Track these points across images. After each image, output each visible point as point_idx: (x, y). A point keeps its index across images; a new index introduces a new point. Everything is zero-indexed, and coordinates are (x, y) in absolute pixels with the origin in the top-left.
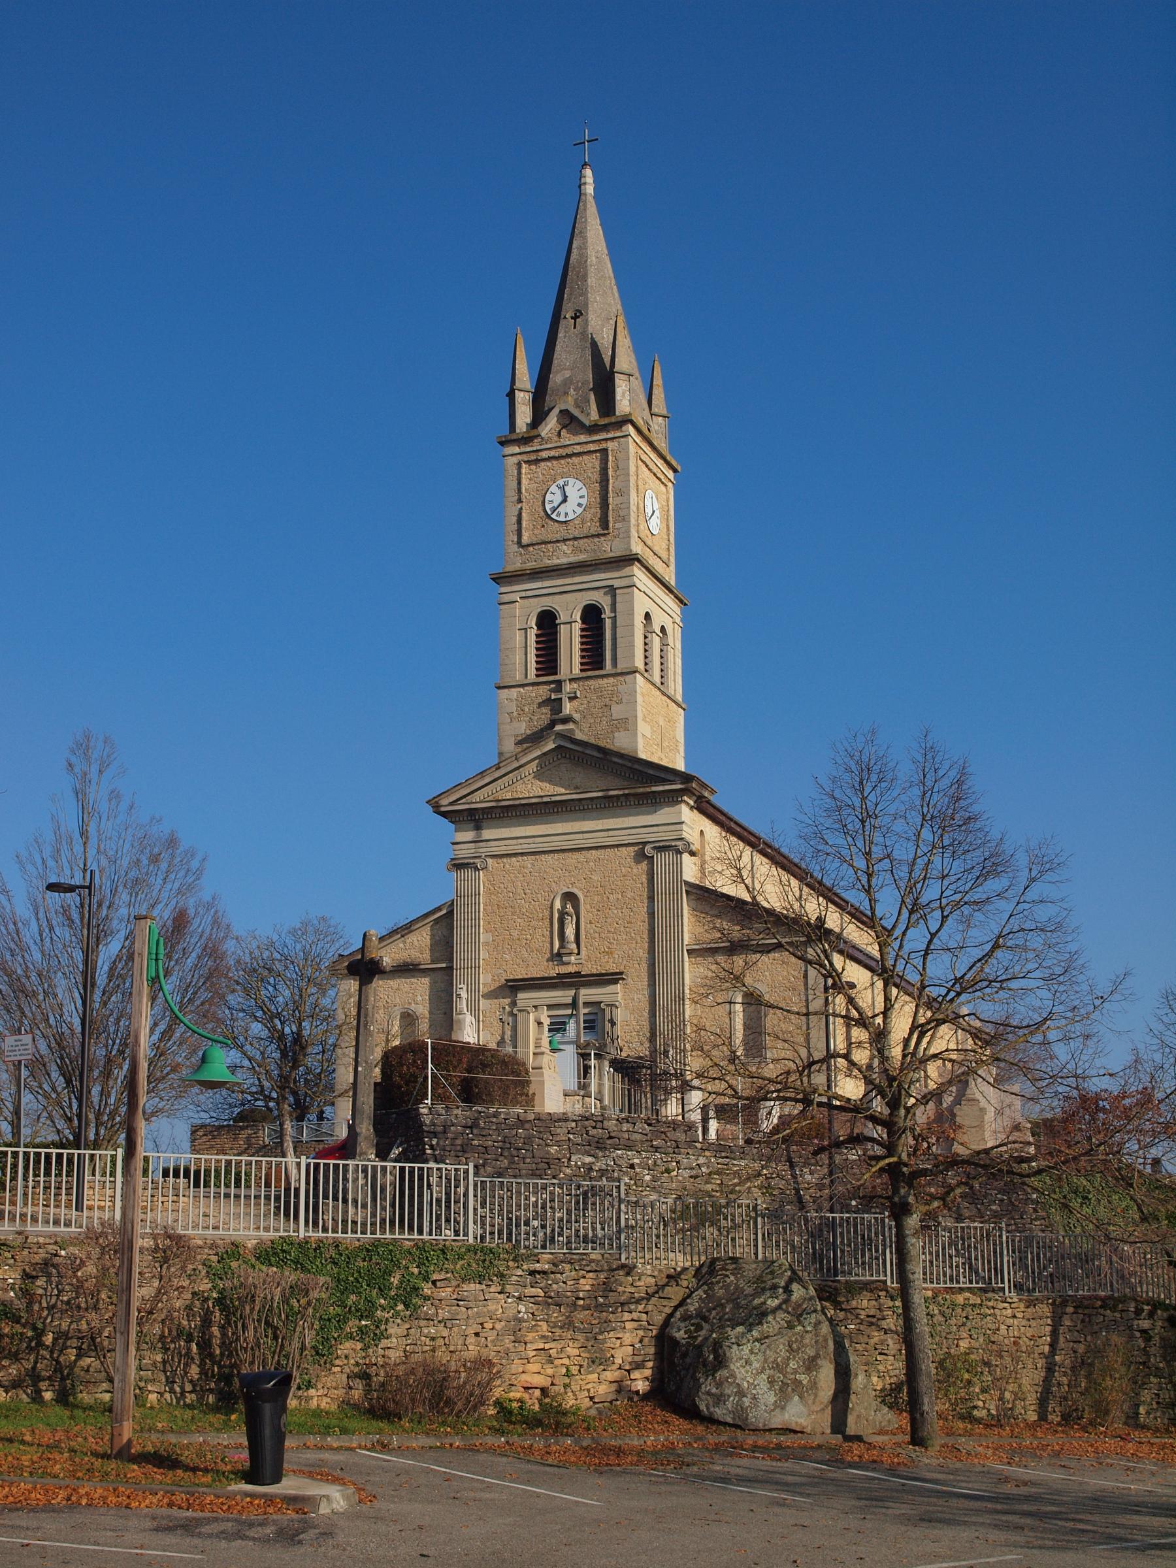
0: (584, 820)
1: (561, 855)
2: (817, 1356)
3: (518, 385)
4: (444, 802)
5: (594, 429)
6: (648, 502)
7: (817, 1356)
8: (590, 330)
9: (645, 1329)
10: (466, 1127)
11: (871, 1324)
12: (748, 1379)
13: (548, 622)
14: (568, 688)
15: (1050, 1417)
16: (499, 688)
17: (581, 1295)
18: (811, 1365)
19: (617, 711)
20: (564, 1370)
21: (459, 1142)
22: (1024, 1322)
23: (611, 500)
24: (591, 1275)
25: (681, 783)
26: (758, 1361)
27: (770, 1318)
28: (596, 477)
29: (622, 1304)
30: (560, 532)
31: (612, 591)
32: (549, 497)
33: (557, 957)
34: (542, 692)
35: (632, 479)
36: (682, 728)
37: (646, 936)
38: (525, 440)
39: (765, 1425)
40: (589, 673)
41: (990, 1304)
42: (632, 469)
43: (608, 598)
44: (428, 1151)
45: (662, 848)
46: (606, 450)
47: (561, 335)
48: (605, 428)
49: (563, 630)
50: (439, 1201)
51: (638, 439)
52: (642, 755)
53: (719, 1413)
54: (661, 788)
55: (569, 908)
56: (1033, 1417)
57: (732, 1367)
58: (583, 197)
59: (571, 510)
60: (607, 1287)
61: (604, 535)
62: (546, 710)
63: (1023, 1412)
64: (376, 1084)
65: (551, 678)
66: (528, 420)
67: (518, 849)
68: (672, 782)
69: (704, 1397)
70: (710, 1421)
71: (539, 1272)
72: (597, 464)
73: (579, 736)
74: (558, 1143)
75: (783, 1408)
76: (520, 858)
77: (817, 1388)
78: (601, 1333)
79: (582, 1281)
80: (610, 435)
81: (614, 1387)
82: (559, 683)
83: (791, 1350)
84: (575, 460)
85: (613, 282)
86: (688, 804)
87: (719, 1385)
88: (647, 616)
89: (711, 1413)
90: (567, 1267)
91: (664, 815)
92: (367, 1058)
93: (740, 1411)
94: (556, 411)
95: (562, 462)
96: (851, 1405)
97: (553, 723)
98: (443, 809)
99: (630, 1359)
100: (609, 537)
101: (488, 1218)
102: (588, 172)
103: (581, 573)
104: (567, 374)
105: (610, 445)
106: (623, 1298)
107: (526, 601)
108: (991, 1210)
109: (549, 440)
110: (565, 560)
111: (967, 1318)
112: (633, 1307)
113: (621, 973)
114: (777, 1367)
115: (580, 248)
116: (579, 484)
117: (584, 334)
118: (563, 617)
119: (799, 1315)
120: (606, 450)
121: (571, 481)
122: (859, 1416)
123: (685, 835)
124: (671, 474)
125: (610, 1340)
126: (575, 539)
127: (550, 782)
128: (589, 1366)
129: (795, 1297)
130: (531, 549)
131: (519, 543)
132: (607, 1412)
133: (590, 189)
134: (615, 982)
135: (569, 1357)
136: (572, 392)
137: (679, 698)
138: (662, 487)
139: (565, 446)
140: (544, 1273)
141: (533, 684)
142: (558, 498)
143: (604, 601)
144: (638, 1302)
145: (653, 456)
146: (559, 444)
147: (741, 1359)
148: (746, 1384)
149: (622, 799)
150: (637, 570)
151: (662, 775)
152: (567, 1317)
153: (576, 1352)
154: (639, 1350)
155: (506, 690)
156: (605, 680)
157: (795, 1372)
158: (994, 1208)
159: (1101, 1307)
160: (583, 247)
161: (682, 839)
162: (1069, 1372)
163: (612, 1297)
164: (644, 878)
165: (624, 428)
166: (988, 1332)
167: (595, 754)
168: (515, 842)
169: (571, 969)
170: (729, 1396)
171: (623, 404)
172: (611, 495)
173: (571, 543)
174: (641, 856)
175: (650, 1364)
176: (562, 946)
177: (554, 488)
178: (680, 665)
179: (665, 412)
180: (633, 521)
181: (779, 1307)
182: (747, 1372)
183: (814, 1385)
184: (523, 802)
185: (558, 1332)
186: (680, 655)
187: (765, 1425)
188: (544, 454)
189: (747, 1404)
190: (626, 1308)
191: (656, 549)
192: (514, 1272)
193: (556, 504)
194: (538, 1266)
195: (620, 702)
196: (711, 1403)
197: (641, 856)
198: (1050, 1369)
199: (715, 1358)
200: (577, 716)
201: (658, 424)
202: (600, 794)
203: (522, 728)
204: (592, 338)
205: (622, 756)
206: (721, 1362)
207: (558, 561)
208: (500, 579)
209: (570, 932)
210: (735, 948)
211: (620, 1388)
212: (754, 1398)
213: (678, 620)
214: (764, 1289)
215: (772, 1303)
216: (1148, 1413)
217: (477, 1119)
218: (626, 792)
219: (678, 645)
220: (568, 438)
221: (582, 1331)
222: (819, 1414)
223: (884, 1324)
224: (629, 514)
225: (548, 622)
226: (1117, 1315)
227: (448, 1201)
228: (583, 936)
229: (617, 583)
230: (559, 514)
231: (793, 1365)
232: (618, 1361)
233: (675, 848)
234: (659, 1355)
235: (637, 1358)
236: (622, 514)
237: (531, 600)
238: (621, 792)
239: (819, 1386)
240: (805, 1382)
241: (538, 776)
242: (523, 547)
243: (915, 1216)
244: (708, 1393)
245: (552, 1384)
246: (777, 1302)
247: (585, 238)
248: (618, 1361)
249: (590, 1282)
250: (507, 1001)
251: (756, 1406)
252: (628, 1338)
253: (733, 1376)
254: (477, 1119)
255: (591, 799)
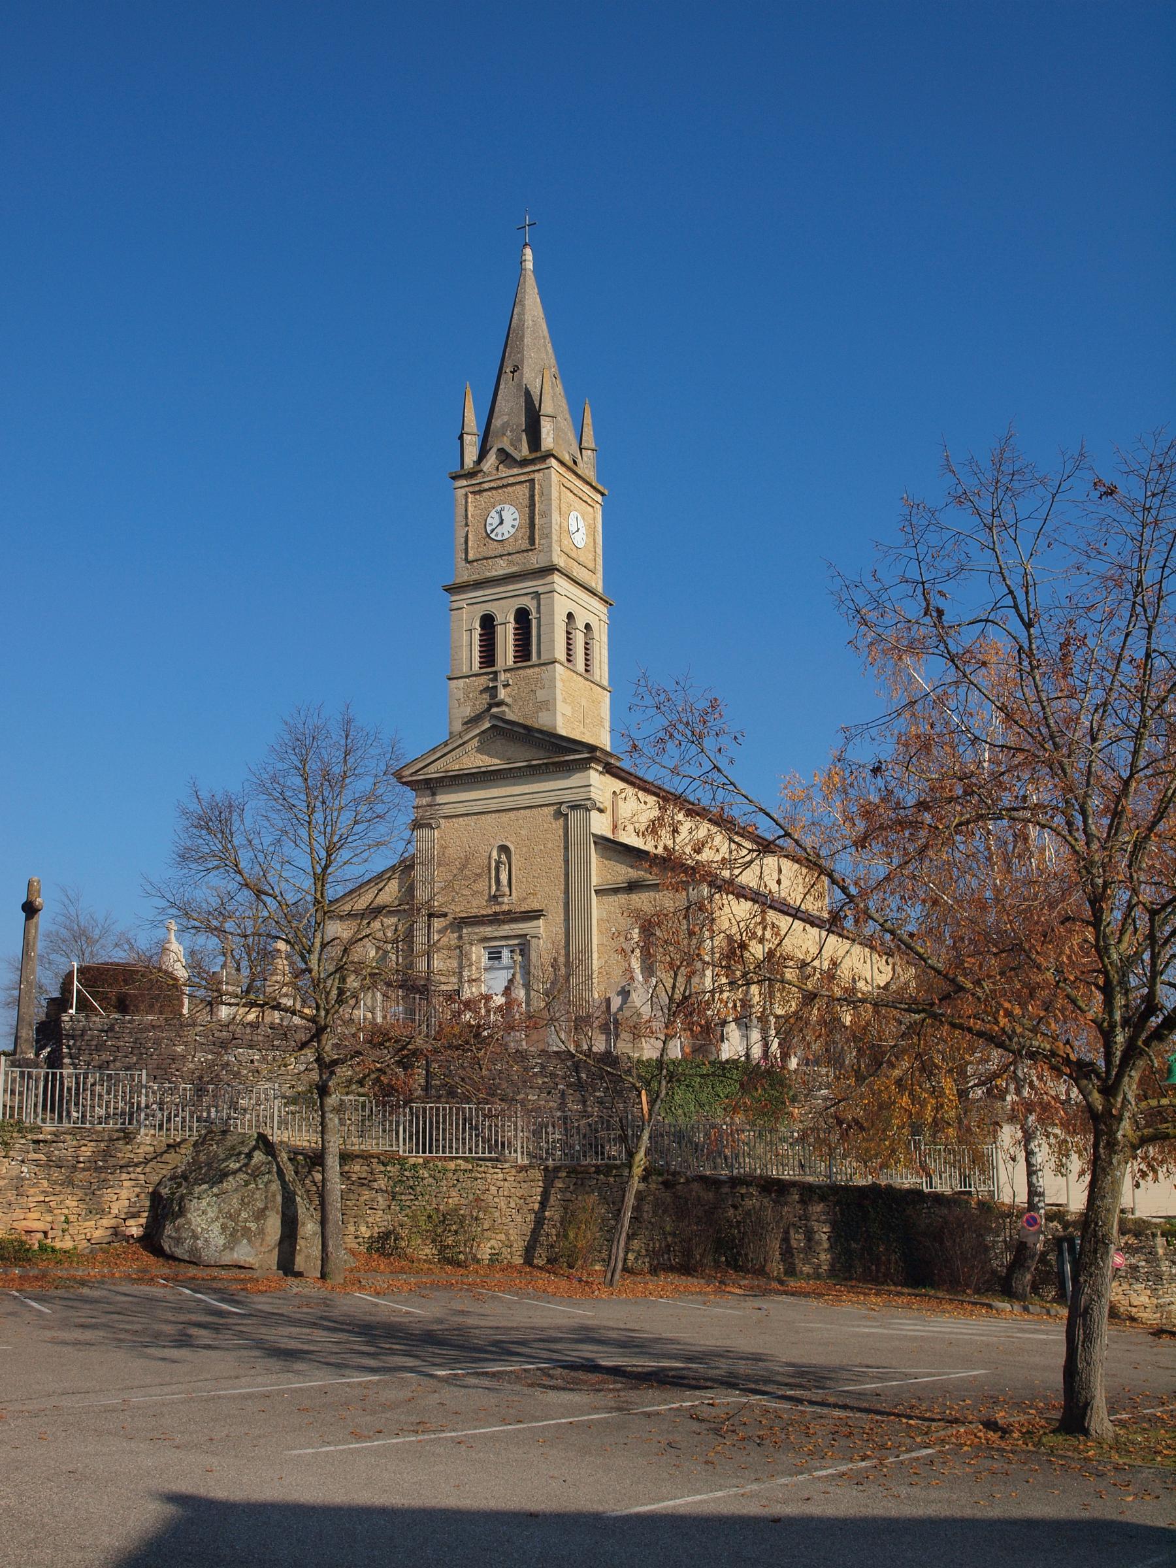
0: (514, 785)
1: (497, 815)
2: (266, 1208)
3: (466, 429)
4: (407, 773)
5: (524, 463)
6: (572, 521)
7: (266, 1208)
8: (525, 382)
9: (142, 1186)
10: (102, 1031)
11: (363, 1184)
12: (203, 1226)
13: (488, 623)
14: (502, 677)
15: (535, 1261)
16: (450, 679)
17: (81, 1159)
18: (260, 1215)
19: (541, 695)
20: (63, 1218)
21: (94, 1043)
22: (515, 1184)
23: (537, 521)
24: (92, 1144)
25: (589, 753)
26: (213, 1212)
27: (230, 1178)
28: (526, 502)
29: (121, 1167)
30: (496, 549)
31: (537, 596)
32: (489, 521)
33: (494, 898)
34: (483, 681)
35: (555, 504)
36: (608, 706)
37: (562, 880)
38: (472, 474)
39: (215, 1262)
40: (519, 665)
41: (481, 1169)
42: (555, 494)
43: (535, 602)
44: (65, 1050)
45: (574, 807)
46: (533, 480)
47: (502, 387)
48: (532, 462)
49: (499, 629)
50: (69, 1089)
51: (562, 470)
52: (562, 732)
53: (179, 1252)
54: (572, 757)
55: (503, 857)
56: (518, 1260)
57: (189, 1215)
58: (523, 272)
59: (506, 531)
60: (107, 1154)
61: (531, 550)
62: (486, 696)
63: (509, 1257)
64: (52, 1000)
65: (489, 670)
66: (475, 458)
67: (464, 810)
68: (581, 752)
69: (166, 1240)
70: (172, 1258)
71: (42, 1141)
72: (527, 491)
73: (510, 716)
74: (186, 1044)
75: (232, 1249)
76: (466, 818)
77: (264, 1234)
78: (99, 1189)
79: (83, 1148)
80: (537, 468)
81: (109, 1232)
82: (495, 673)
83: (243, 1203)
84: (510, 489)
85: (548, 339)
86: (597, 770)
87: (177, 1230)
88: (570, 616)
89: (173, 1253)
90: (68, 1137)
91: (576, 779)
92: (28, 977)
93: (194, 1250)
94: (494, 450)
95: (500, 491)
96: (298, 1248)
97: (491, 706)
98: (404, 780)
99: (126, 1210)
100: (535, 552)
101: (112, 1103)
102: (528, 252)
103: (513, 583)
104: (506, 418)
105: (537, 476)
106: (122, 1163)
107: (471, 607)
108: (594, 1096)
109: (490, 474)
110: (501, 572)
111: (458, 1181)
112: (131, 1169)
113: (542, 911)
114: (230, 1216)
115: (519, 314)
116: (513, 509)
117: (519, 385)
118: (499, 619)
119: (255, 1175)
120: (533, 480)
121: (507, 507)
122: (308, 1257)
123: (593, 795)
124: (599, 498)
125: (109, 1195)
126: (509, 554)
127: (489, 755)
128: (86, 1215)
129: (255, 1161)
130: (475, 564)
131: (466, 559)
132: (97, 1252)
133: (529, 265)
134: (537, 918)
135: (68, 1208)
136: (508, 433)
137: (605, 683)
138: (589, 508)
139: (502, 478)
140: (45, 1141)
141: (476, 675)
142: (497, 521)
143: (530, 604)
144: (137, 1165)
145: (579, 483)
146: (497, 477)
147: (198, 1210)
148: (199, 1230)
149: (543, 767)
150: (557, 578)
151: (572, 746)
152: (67, 1177)
153: (76, 1204)
154: (135, 1202)
155: (455, 681)
156: (532, 670)
157: (246, 1220)
158: (598, 1094)
159: (595, 1172)
160: (522, 313)
161: (590, 799)
162: (558, 1224)
163: (111, 1161)
164: (561, 832)
165: (548, 461)
166: (478, 1192)
167: (522, 731)
168: (461, 805)
169: (505, 908)
170: (186, 1239)
171: (548, 441)
172: (537, 517)
173: (506, 557)
174: (559, 814)
175: (146, 1214)
176: (497, 890)
177: (493, 514)
178: (606, 654)
179: (593, 446)
180: (555, 537)
181: (240, 1169)
182: (202, 1220)
183: (261, 1232)
184: (466, 772)
185: (58, 1188)
186: (606, 647)
187: (215, 1262)
188: (486, 486)
189: (200, 1245)
190: (124, 1170)
191: (581, 559)
192: (16, 1141)
193: (494, 527)
194: (41, 1137)
195: (542, 688)
196: (173, 1244)
197: (559, 814)
198: (539, 1222)
199: (180, 1209)
200: (508, 700)
201: (588, 459)
202: (525, 764)
203: (468, 711)
204: (526, 389)
205: (541, 732)
206: (182, 1212)
207: (496, 573)
208: (452, 589)
209: (504, 881)
210: (633, 887)
211: (116, 1232)
212: (206, 1240)
213: (605, 618)
214: (232, 1155)
215: (234, 1166)
216: (636, 1259)
217: (113, 1025)
218: (545, 761)
219: (605, 639)
220: (504, 472)
221: (82, 1188)
222: (266, 1255)
223: (375, 1185)
224: (551, 532)
225: (488, 623)
226: (612, 1179)
227: (77, 1089)
228: (513, 881)
229: (541, 590)
230: (497, 535)
231: (244, 1215)
232: (115, 1211)
233: (584, 806)
234: (153, 1208)
235: (132, 1210)
236: (545, 532)
237: (475, 606)
238: (541, 762)
239: (266, 1231)
240: (253, 1229)
241: (479, 750)
242: (469, 562)
243: (334, 1096)
244: (169, 1237)
245: (52, 1229)
246: (238, 1165)
247: (523, 305)
248: (115, 1211)
249: (91, 1149)
250: (456, 935)
251: (208, 1247)
252: (124, 1194)
253: (190, 1223)
254: (113, 1025)
255: (519, 768)
